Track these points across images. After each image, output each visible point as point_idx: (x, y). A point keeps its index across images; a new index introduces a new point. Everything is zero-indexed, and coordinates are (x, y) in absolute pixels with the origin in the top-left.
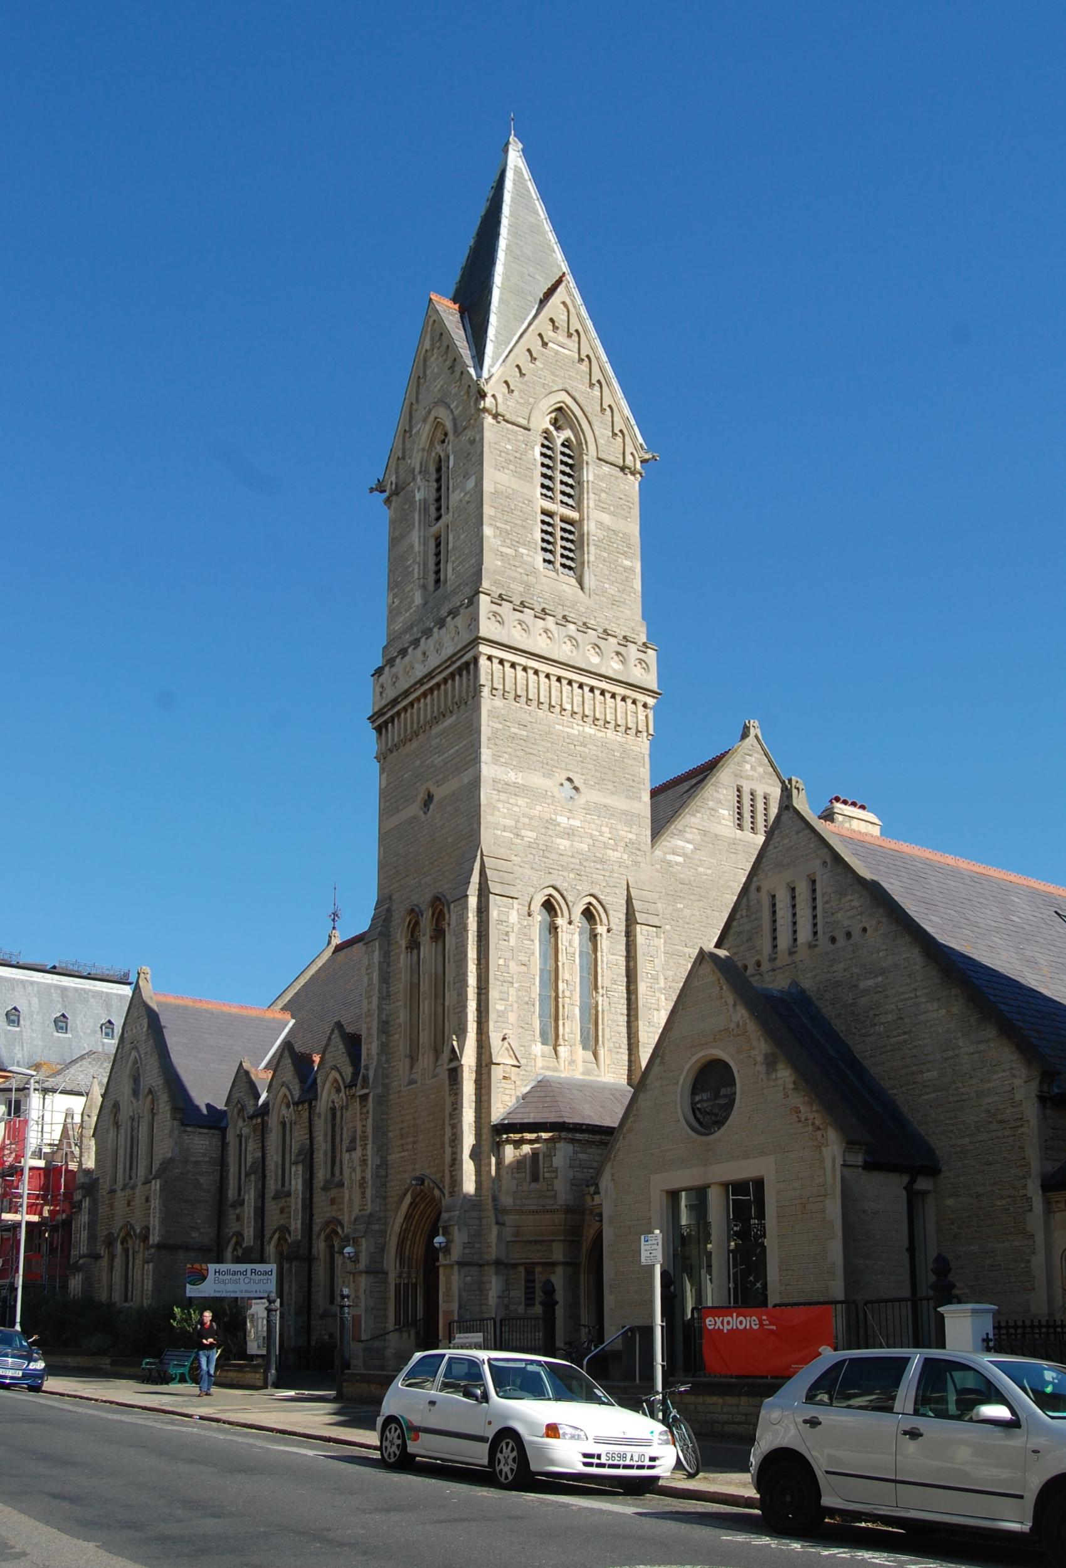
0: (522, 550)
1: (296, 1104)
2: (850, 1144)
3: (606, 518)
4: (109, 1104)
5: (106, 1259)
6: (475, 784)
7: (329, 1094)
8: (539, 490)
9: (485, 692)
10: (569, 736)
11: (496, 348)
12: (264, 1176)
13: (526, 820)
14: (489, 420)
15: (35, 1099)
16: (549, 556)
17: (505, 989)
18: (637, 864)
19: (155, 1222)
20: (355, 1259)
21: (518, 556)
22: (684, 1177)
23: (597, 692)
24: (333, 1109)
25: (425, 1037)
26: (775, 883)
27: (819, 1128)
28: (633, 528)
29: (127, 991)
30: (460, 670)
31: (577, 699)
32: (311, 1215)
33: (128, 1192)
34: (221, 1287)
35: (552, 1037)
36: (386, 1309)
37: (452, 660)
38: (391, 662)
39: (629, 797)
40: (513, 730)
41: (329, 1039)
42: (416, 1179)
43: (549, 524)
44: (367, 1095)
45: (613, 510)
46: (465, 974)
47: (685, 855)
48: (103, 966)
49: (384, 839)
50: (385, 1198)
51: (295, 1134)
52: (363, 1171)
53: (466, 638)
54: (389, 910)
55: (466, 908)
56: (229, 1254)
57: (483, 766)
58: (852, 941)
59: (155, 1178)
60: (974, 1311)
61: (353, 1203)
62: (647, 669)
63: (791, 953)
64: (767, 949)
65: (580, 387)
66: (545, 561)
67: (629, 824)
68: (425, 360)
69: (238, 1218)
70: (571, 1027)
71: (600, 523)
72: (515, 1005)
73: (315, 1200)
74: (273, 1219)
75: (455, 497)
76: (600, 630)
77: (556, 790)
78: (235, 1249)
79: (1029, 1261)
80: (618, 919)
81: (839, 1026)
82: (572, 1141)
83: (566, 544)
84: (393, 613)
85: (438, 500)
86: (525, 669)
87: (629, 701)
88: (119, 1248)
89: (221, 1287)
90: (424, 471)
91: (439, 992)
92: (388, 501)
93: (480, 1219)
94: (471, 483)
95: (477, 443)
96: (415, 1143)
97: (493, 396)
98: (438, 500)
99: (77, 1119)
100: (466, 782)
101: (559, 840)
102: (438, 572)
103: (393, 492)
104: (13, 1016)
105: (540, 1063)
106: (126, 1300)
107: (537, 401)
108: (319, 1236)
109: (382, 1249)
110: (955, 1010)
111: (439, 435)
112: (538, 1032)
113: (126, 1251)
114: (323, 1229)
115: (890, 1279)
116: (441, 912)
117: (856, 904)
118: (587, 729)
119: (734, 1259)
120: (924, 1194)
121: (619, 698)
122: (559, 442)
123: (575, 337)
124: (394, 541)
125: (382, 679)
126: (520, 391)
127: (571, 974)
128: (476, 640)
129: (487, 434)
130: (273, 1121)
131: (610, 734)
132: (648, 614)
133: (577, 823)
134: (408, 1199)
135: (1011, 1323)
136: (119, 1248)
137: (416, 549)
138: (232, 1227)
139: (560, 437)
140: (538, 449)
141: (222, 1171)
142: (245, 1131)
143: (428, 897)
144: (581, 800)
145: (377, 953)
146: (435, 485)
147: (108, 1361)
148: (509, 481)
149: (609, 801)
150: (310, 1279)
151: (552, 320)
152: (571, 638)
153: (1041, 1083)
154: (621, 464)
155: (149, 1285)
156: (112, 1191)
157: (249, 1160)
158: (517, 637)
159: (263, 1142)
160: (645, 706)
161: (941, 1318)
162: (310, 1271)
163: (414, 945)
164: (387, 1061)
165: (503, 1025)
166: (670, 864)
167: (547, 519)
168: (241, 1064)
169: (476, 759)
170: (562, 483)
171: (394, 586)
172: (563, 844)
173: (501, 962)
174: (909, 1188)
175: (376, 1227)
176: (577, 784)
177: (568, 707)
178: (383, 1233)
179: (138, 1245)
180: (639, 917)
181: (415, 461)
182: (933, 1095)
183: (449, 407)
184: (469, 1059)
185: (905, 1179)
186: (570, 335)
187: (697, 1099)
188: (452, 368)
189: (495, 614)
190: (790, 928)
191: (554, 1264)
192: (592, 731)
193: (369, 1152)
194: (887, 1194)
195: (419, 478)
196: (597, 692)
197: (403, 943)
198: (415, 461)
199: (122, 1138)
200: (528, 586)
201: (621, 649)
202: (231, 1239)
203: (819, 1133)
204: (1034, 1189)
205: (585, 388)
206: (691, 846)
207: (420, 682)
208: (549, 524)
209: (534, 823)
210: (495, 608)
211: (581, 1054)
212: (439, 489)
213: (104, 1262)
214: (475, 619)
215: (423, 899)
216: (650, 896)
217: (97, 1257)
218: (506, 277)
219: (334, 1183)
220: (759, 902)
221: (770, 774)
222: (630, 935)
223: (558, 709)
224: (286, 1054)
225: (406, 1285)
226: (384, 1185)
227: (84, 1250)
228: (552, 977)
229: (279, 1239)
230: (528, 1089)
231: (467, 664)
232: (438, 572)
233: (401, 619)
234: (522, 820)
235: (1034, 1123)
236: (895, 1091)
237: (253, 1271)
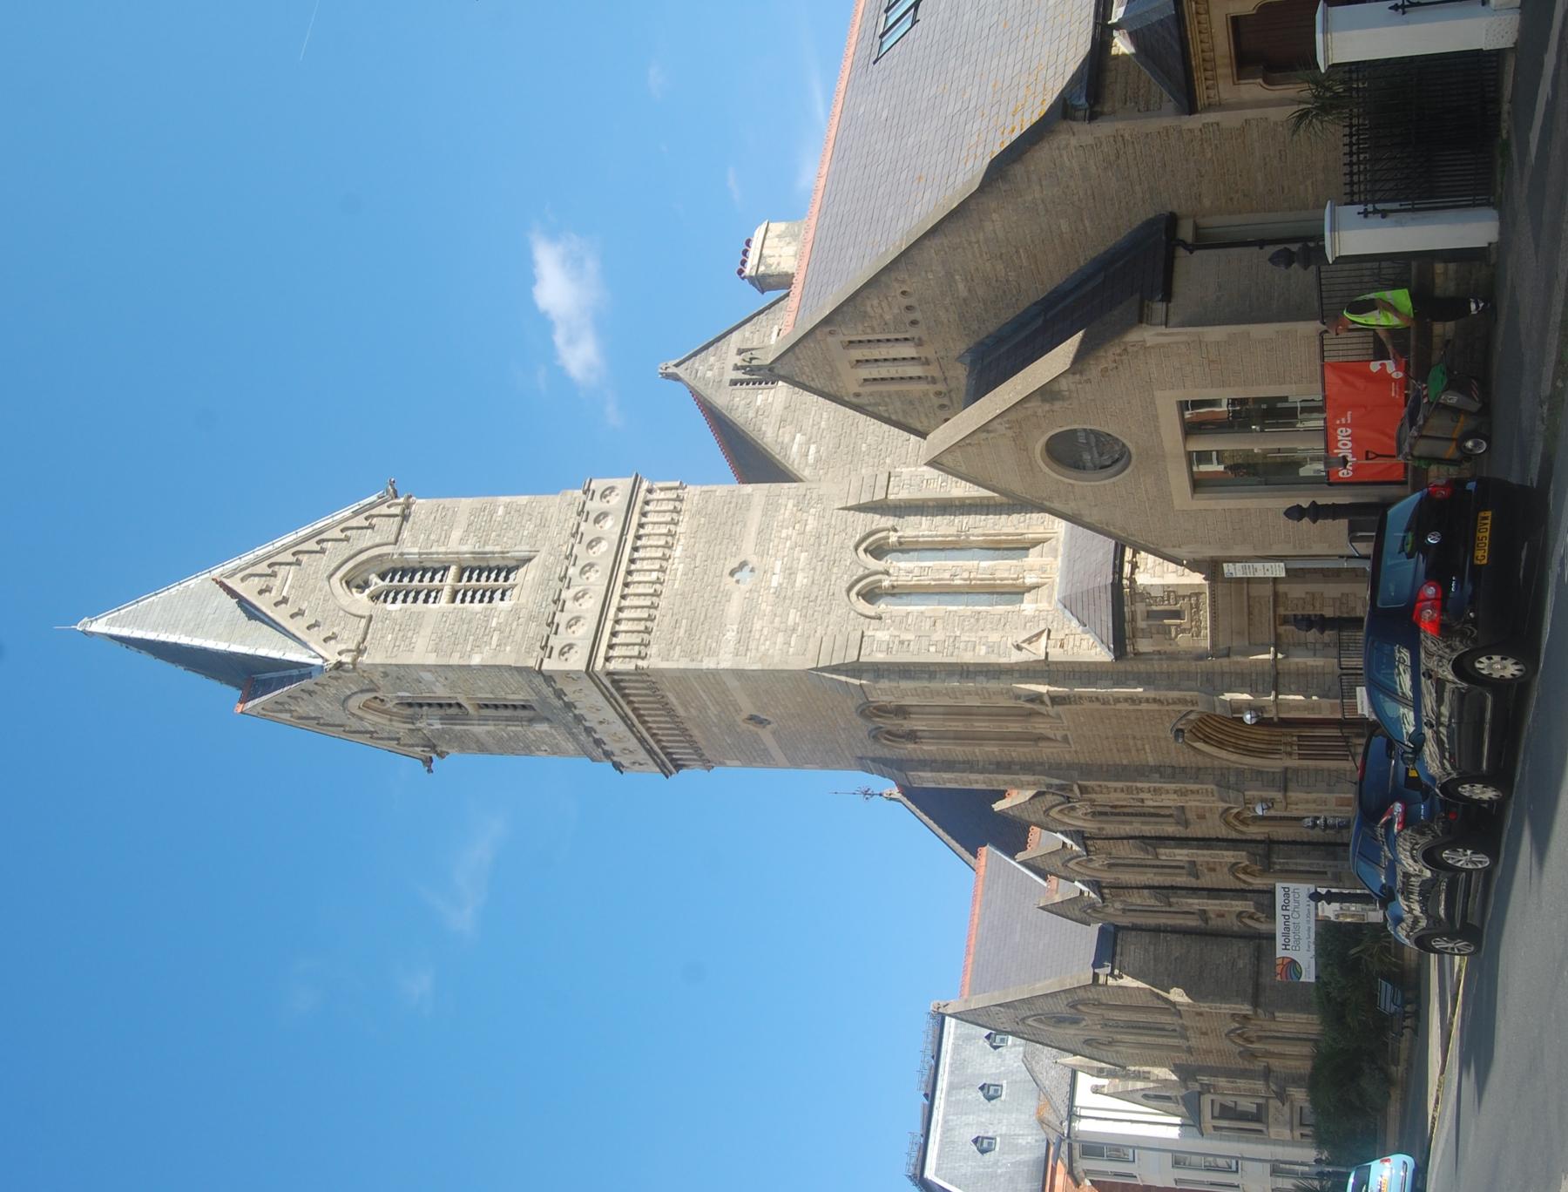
2: (1142, 318)
3: (456, 534)
4: (1087, 1050)
5: (1271, 1061)
6: (739, 674)
8: (430, 605)
12: (1172, 888)
14: (365, 659)
15: (1081, 1126)
16: (498, 595)
17: (962, 645)
19: (1226, 1008)
20: (1270, 803)
21: (498, 629)
22: (1179, 479)
24: (1094, 814)
25: (1015, 727)
26: (851, 380)
28: (465, 505)
30: (619, 689)
31: (646, 565)
32: (1218, 839)
34: (1304, 944)
35: (1016, 592)
36: (1329, 770)
37: (608, 697)
42: (1176, 737)
44: (1080, 787)
45: (447, 526)
47: (809, 442)
48: (924, 1042)
49: (795, 762)
50: (1199, 769)
51: (1123, 854)
54: (873, 760)
56: (1263, 927)
57: (722, 666)
58: (916, 304)
60: (1325, 31)
61: (1204, 805)
62: (612, 489)
63: (927, 362)
64: (923, 386)
65: (325, 563)
68: (300, 718)
69: (1202, 817)
70: (1003, 569)
71: (462, 541)
73: (1200, 835)
74: (1223, 880)
75: (441, 692)
78: (1258, 920)
79: (1276, 123)
81: (1008, 315)
83: (487, 573)
84: (556, 750)
85: (440, 705)
89: (1304, 944)
90: (412, 719)
92: (441, 755)
93: (1223, 674)
94: (427, 676)
95: (386, 671)
97: (340, 654)
99: (1104, 1082)
100: (737, 684)
101: (798, 584)
103: (431, 750)
104: (983, 1145)
105: (1043, 605)
109: (1259, 773)
110: (993, 205)
111: (376, 704)
112: (1009, 608)
113: (1260, 1038)
116: (878, 708)
117: (875, 302)
119: (1272, 426)
121: (644, 520)
122: (381, 583)
124: (482, 748)
128: (589, 672)
130: (1108, 877)
132: (555, 490)
133: (778, 564)
134: (1199, 745)
135: (1347, 140)
137: (492, 728)
140: (389, 606)
141: (1165, 931)
142: (1118, 905)
143: (860, 721)
144: (754, 560)
145: (921, 774)
147: (1393, 1068)
148: (424, 637)
149: (753, 530)
150: (1294, 843)
151: (309, 628)
152: (582, 572)
153: (1074, 119)
154: (398, 519)
155: (1302, 1017)
156: (1189, 1050)
157: (1153, 902)
158: (584, 632)
160: (650, 491)
161: (1341, 260)
162: (1283, 842)
163: (912, 736)
164: (1042, 764)
166: (817, 460)
167: (460, 596)
168: (1043, 908)
169: (714, 673)
171: (528, 749)
172: (801, 580)
174: (1191, 248)
175: (1232, 780)
176: (736, 565)
177: (654, 576)
178: (1240, 773)
180: (879, 496)
181: (401, 728)
182: (1087, 223)
183: (349, 697)
185: (1181, 252)
186: (274, 575)
187: (1089, 464)
189: (562, 653)
193: (1146, 785)
194: (1197, 273)
195: (419, 725)
197: (911, 746)
200: (531, 618)
201: (592, 517)
203: (1130, 349)
204: (1194, 122)
205: (325, 558)
207: (631, 727)
210: (555, 653)
211: (1033, 558)
213: (1275, 1063)
214: (567, 674)
215: (862, 727)
216: (855, 484)
218: (218, 637)
219: (1181, 816)
220: (871, 394)
226: (1184, 769)
229: (1246, 873)
231: (614, 682)
232: (515, 707)
235: (1120, 125)
237: (1285, 908)
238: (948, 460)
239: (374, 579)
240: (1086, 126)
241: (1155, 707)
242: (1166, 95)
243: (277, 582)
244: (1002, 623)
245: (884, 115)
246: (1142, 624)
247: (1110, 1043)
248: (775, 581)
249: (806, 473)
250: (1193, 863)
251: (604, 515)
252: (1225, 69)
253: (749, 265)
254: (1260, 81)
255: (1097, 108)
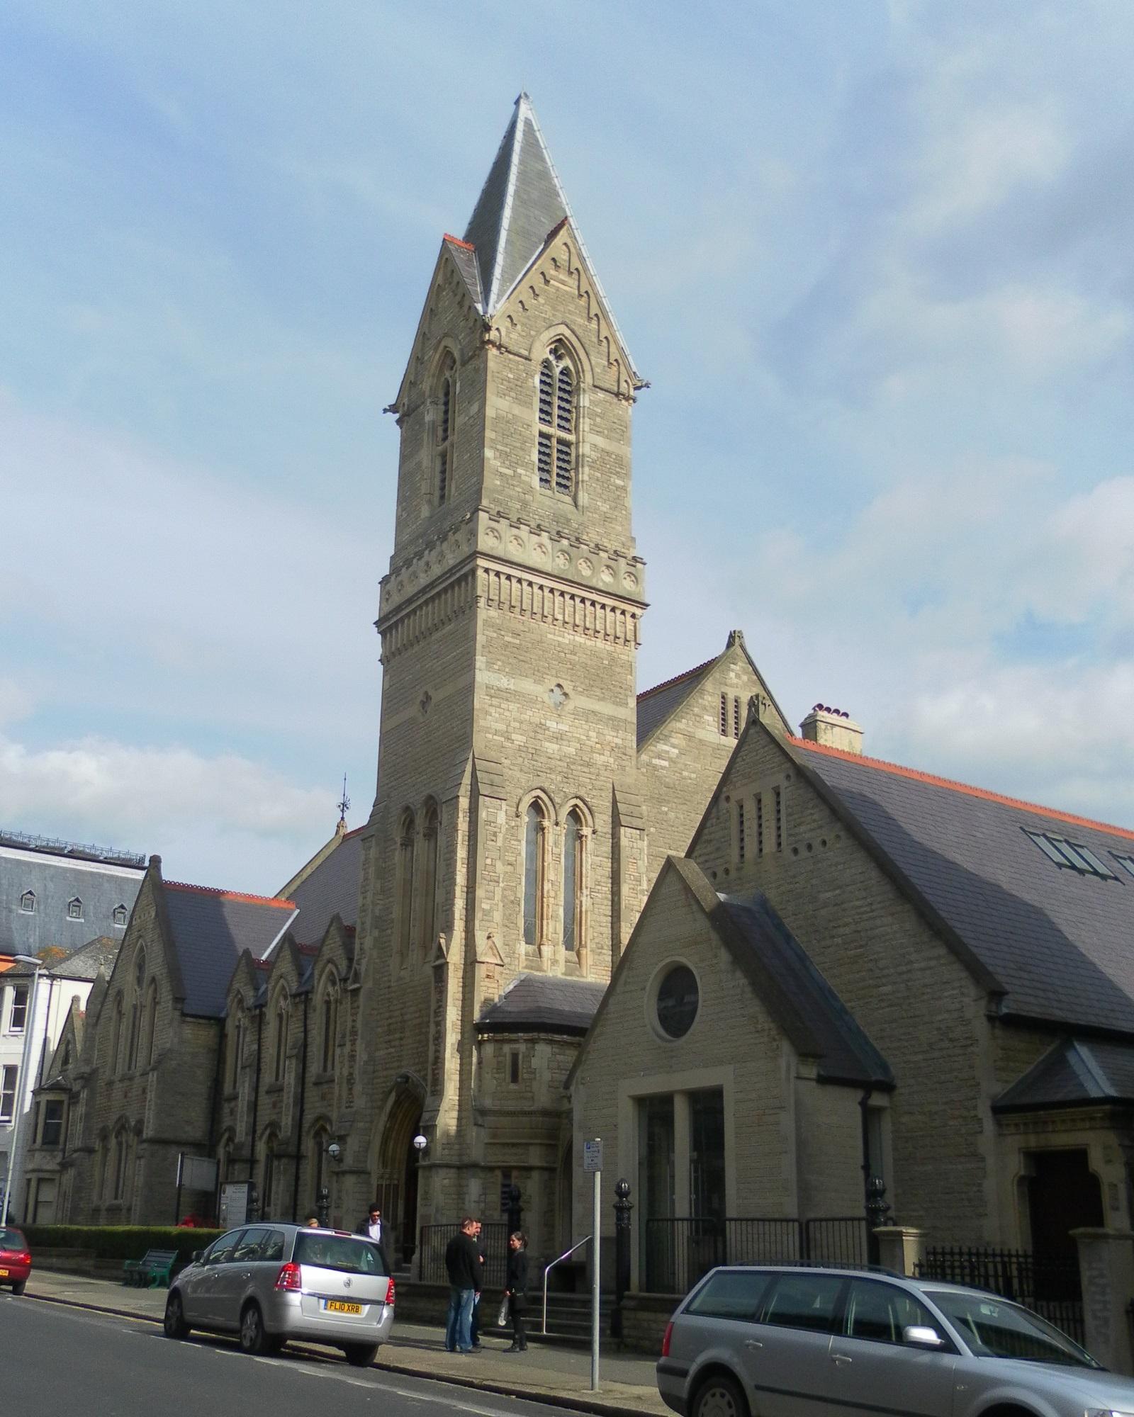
0: (519, 471)
1: (294, 996)
3: (600, 441)
6: (469, 689)
7: (326, 988)
9: (482, 602)
10: (560, 644)
11: (502, 285)
12: (259, 1070)
13: (517, 725)
14: (493, 352)
15: (43, 986)
16: (545, 476)
18: (623, 768)
21: (516, 476)
22: (652, 1085)
23: (588, 603)
26: (742, 792)
27: (775, 1040)
29: (140, 875)
30: (459, 581)
31: (569, 610)
32: (302, 1111)
33: (127, 1083)
35: (533, 935)
37: (451, 571)
38: (395, 570)
39: (615, 703)
40: (506, 638)
41: (328, 932)
43: (546, 446)
46: (454, 873)
47: (670, 760)
52: (351, 1067)
53: (466, 550)
55: (457, 808)
59: (153, 1069)
64: (735, 857)
66: (541, 480)
67: (616, 729)
70: (554, 927)
71: (594, 447)
72: (501, 905)
74: (265, 1116)
75: (460, 420)
76: (592, 545)
77: (546, 697)
78: (227, 1145)
79: (980, 1185)
80: (603, 821)
82: (551, 1042)
85: (446, 421)
86: (520, 581)
87: (618, 612)
88: (113, 1142)
91: (430, 892)
92: (399, 422)
96: (401, 1039)
98: (446, 421)
101: (547, 744)
102: (443, 488)
106: (116, 1198)
107: (539, 333)
108: (309, 1132)
113: (120, 1144)
114: (313, 1125)
115: (844, 1196)
117: (815, 817)
118: (577, 638)
120: (879, 1110)
121: (608, 609)
122: (557, 371)
123: (575, 276)
125: (388, 587)
126: (523, 325)
127: (555, 875)
128: (475, 554)
129: (491, 364)
131: (600, 644)
136: (113, 1142)
138: (227, 1122)
139: (558, 368)
144: (570, 705)
146: (443, 407)
150: (297, 1178)
151: (554, 259)
153: (989, 1002)
154: (616, 389)
156: (110, 1084)
158: (514, 552)
159: (260, 1034)
162: (298, 1169)
163: (408, 843)
165: (488, 924)
166: (655, 767)
167: (545, 441)
170: (560, 407)
172: (551, 747)
173: (489, 861)
174: (863, 1104)
176: (566, 690)
177: (560, 617)
179: (131, 1138)
181: (426, 386)
184: (455, 957)
188: (461, 304)
189: (493, 530)
190: (756, 839)
191: (529, 1169)
192: (582, 640)
196: (588, 603)
198: (426, 386)
199: (123, 1027)
202: (222, 1135)
204: (984, 1112)
206: (676, 751)
207: (423, 591)
208: (546, 446)
209: (524, 727)
210: (494, 524)
212: (446, 412)
213: (98, 1157)
214: (473, 534)
217: (90, 1151)
218: (514, 219)
221: (754, 682)
222: (615, 837)
223: (550, 619)
224: (286, 945)
225: (388, 1186)
227: (78, 1143)
228: (536, 877)
230: (511, 987)
231: (465, 576)
232: (443, 488)
233: (409, 530)
234: (513, 724)
236: (853, 1004)
238: (671, 878)
239: (562, 365)
240: (982, 1012)
241: (431, 1058)
242: (1011, 1085)
243: (563, 277)
244: (509, 921)
245: (978, 834)
246: (507, 1048)
247: (120, 1012)
248: (552, 724)
249: (644, 757)
250: (281, 1090)
251: (614, 574)
252: (1033, 1142)
253: (825, 713)
254: (1022, 1173)
255: (997, 1024)
